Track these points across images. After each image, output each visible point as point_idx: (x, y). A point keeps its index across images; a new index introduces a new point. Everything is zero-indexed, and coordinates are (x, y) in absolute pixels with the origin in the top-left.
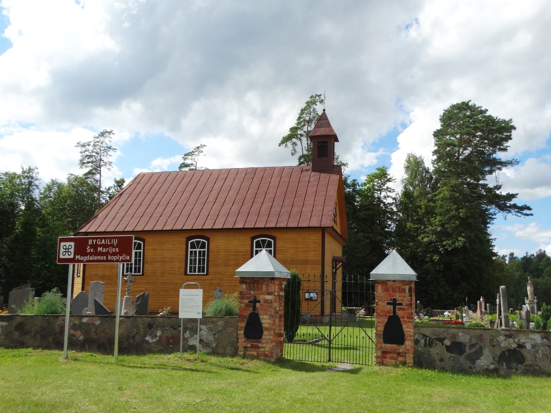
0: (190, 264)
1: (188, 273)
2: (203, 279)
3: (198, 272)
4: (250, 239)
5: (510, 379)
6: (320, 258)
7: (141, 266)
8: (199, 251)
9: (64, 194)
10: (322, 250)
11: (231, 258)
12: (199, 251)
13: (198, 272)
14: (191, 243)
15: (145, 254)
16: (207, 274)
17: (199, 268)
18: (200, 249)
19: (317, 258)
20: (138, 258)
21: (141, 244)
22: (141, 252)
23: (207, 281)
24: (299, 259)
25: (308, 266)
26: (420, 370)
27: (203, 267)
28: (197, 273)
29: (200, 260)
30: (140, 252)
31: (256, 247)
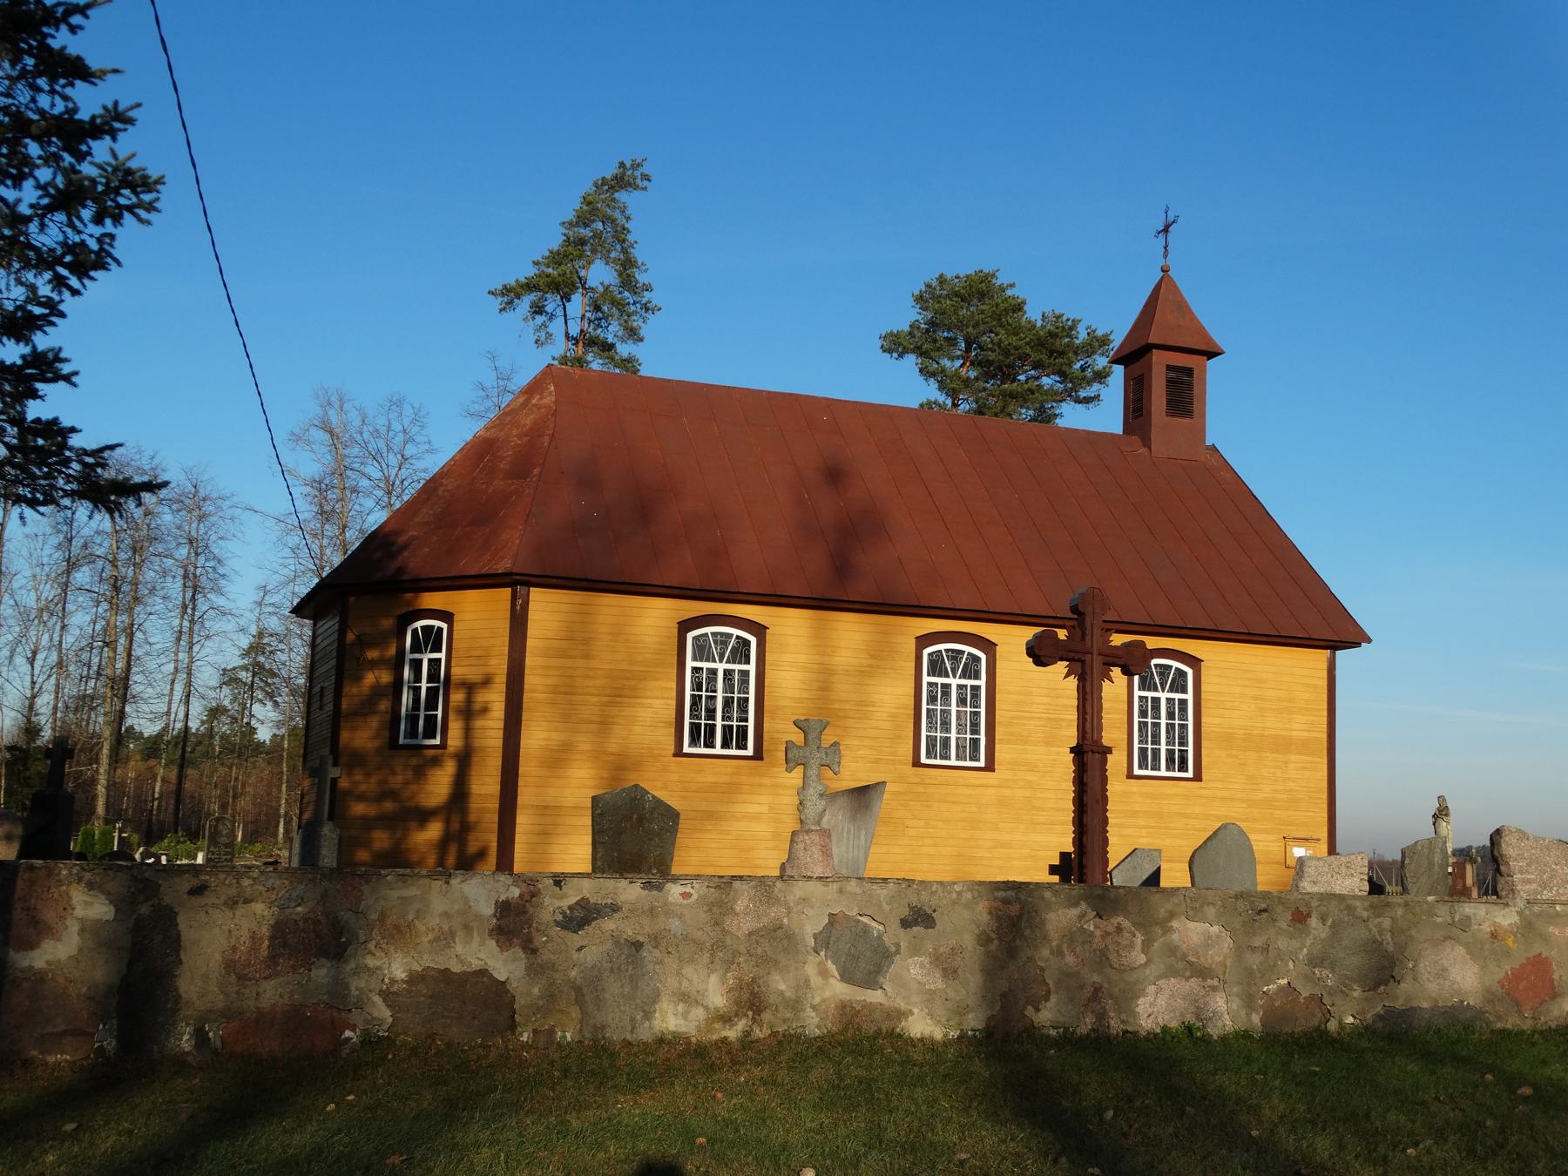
0: (1140, 742)
1: (924, 760)
2: (977, 782)
3: (1168, 769)
4: (677, 626)
5: (603, 1027)
6: (1323, 736)
7: (751, 724)
8: (725, 671)
9: (34, 271)
10: (1328, 709)
11: (1067, 717)
12: (725, 671)
13: (1168, 769)
14: (930, 655)
15: (767, 681)
16: (990, 767)
17: (727, 730)
18: (728, 662)
19: (1315, 735)
20: (1177, 722)
21: (1186, 673)
22: (979, 687)
23: (992, 791)
24: (1266, 733)
25: (1294, 758)
26: (1487, 984)
27: (743, 732)
28: (718, 750)
29: (1170, 727)
30: (976, 689)
31: (695, 659)
